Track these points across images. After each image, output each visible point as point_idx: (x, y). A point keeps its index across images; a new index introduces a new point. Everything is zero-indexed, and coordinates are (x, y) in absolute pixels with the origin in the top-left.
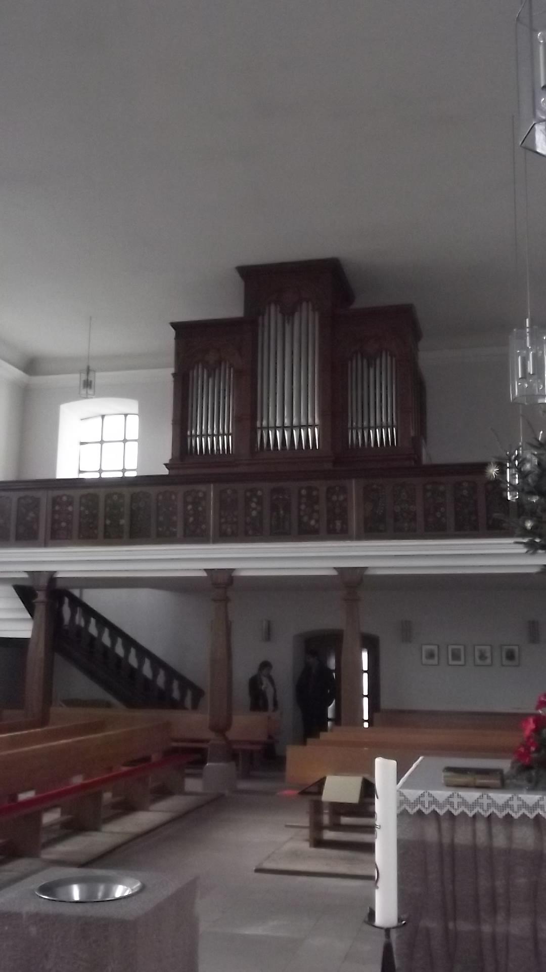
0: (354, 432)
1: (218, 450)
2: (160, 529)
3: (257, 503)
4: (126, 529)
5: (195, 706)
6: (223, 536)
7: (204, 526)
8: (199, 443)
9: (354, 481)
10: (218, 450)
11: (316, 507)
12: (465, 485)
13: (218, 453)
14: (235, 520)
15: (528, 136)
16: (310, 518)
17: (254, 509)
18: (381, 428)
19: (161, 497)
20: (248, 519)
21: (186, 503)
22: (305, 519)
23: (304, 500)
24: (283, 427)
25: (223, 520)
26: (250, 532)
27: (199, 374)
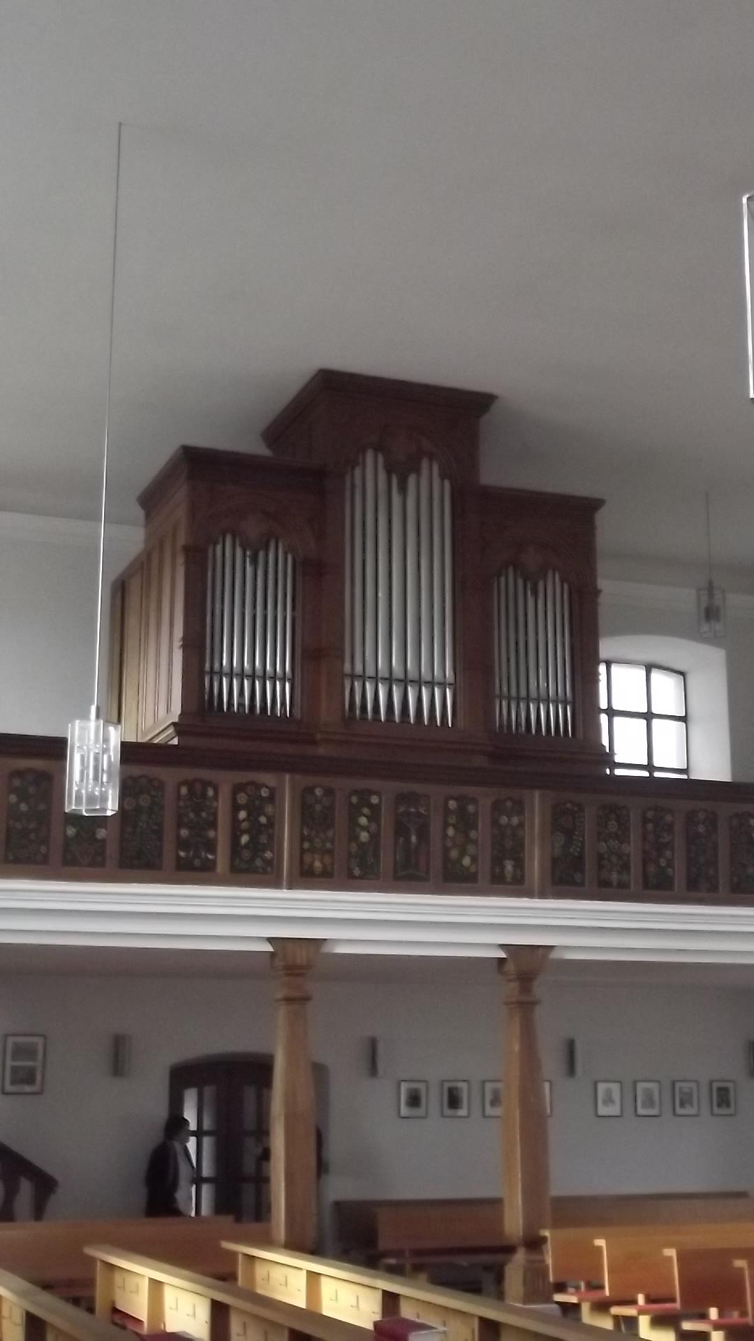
0: (504, 703)
1: (241, 705)
2: (182, 854)
3: (369, 818)
4: (112, 849)
5: (38, 1212)
6: (306, 877)
7: (268, 855)
8: (233, 693)
9: (537, 794)
10: (241, 705)
11: (473, 834)
12: (701, 816)
13: (241, 710)
14: (328, 845)
15: (117, 152)
16: (463, 853)
17: (364, 828)
18: (274, 679)
19: (184, 790)
20: (354, 847)
21: (236, 808)
22: (454, 854)
23: (452, 820)
24: (390, 681)
25: (306, 845)
26: (357, 872)
27: (227, 552)
